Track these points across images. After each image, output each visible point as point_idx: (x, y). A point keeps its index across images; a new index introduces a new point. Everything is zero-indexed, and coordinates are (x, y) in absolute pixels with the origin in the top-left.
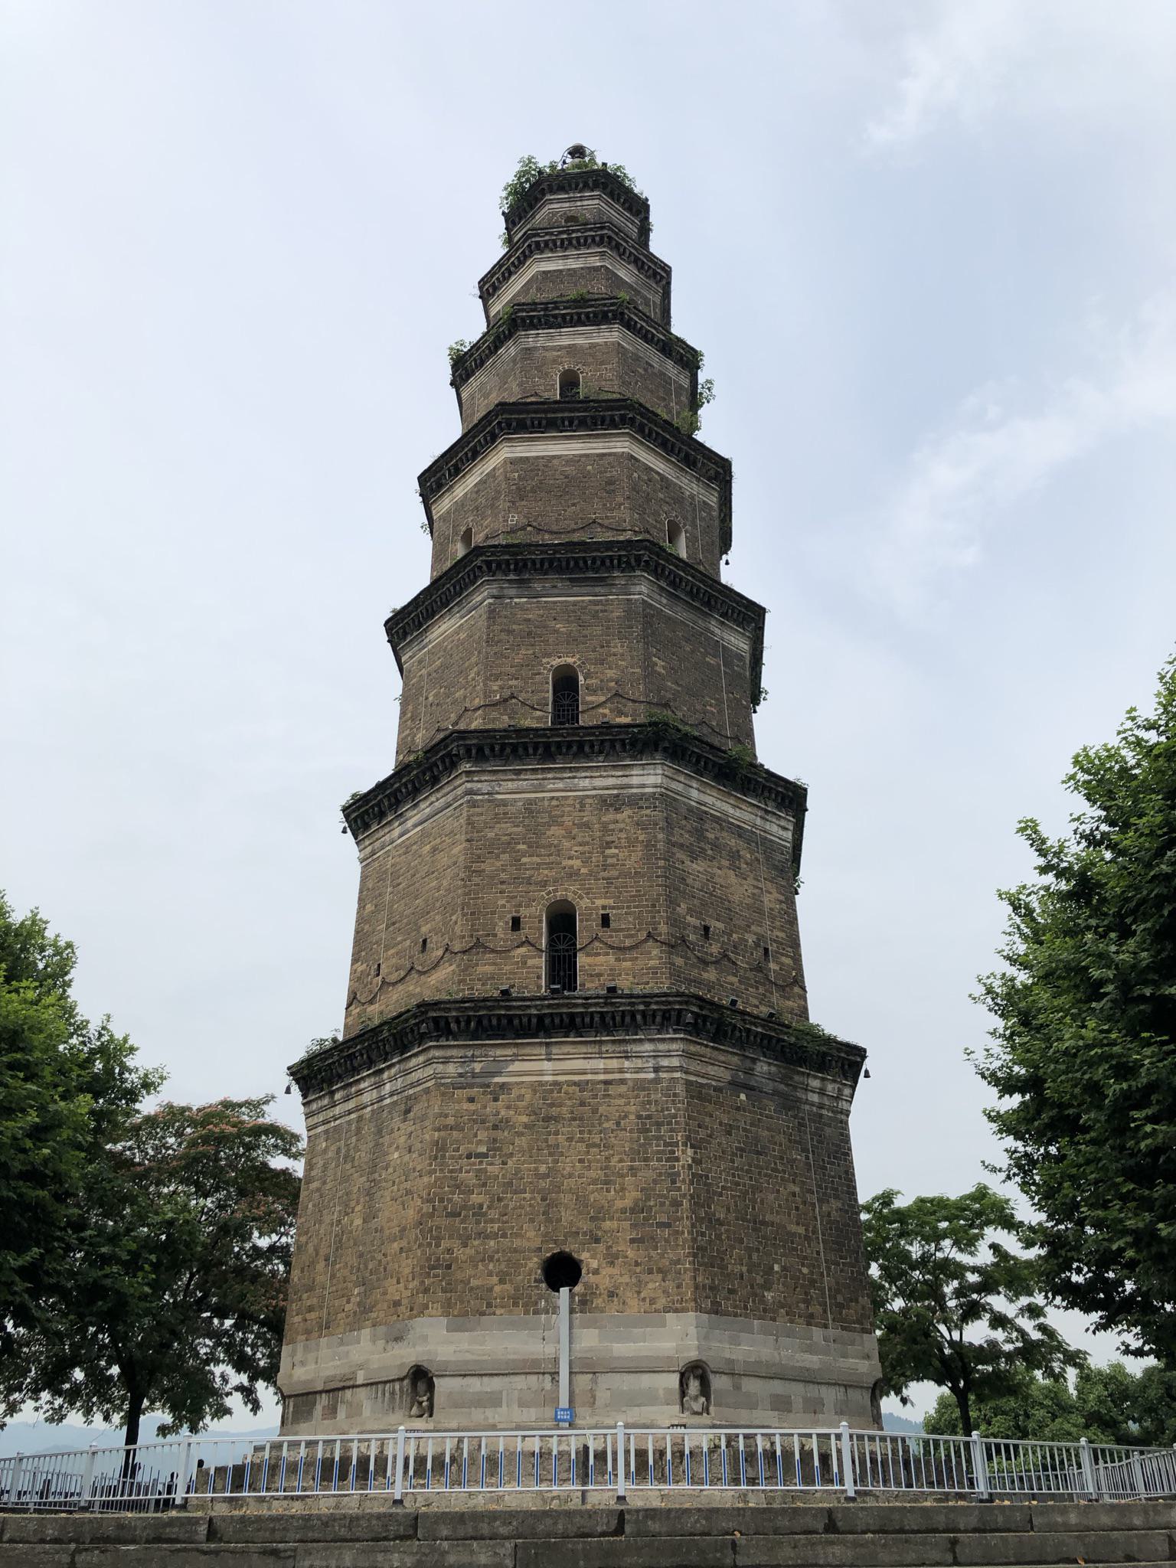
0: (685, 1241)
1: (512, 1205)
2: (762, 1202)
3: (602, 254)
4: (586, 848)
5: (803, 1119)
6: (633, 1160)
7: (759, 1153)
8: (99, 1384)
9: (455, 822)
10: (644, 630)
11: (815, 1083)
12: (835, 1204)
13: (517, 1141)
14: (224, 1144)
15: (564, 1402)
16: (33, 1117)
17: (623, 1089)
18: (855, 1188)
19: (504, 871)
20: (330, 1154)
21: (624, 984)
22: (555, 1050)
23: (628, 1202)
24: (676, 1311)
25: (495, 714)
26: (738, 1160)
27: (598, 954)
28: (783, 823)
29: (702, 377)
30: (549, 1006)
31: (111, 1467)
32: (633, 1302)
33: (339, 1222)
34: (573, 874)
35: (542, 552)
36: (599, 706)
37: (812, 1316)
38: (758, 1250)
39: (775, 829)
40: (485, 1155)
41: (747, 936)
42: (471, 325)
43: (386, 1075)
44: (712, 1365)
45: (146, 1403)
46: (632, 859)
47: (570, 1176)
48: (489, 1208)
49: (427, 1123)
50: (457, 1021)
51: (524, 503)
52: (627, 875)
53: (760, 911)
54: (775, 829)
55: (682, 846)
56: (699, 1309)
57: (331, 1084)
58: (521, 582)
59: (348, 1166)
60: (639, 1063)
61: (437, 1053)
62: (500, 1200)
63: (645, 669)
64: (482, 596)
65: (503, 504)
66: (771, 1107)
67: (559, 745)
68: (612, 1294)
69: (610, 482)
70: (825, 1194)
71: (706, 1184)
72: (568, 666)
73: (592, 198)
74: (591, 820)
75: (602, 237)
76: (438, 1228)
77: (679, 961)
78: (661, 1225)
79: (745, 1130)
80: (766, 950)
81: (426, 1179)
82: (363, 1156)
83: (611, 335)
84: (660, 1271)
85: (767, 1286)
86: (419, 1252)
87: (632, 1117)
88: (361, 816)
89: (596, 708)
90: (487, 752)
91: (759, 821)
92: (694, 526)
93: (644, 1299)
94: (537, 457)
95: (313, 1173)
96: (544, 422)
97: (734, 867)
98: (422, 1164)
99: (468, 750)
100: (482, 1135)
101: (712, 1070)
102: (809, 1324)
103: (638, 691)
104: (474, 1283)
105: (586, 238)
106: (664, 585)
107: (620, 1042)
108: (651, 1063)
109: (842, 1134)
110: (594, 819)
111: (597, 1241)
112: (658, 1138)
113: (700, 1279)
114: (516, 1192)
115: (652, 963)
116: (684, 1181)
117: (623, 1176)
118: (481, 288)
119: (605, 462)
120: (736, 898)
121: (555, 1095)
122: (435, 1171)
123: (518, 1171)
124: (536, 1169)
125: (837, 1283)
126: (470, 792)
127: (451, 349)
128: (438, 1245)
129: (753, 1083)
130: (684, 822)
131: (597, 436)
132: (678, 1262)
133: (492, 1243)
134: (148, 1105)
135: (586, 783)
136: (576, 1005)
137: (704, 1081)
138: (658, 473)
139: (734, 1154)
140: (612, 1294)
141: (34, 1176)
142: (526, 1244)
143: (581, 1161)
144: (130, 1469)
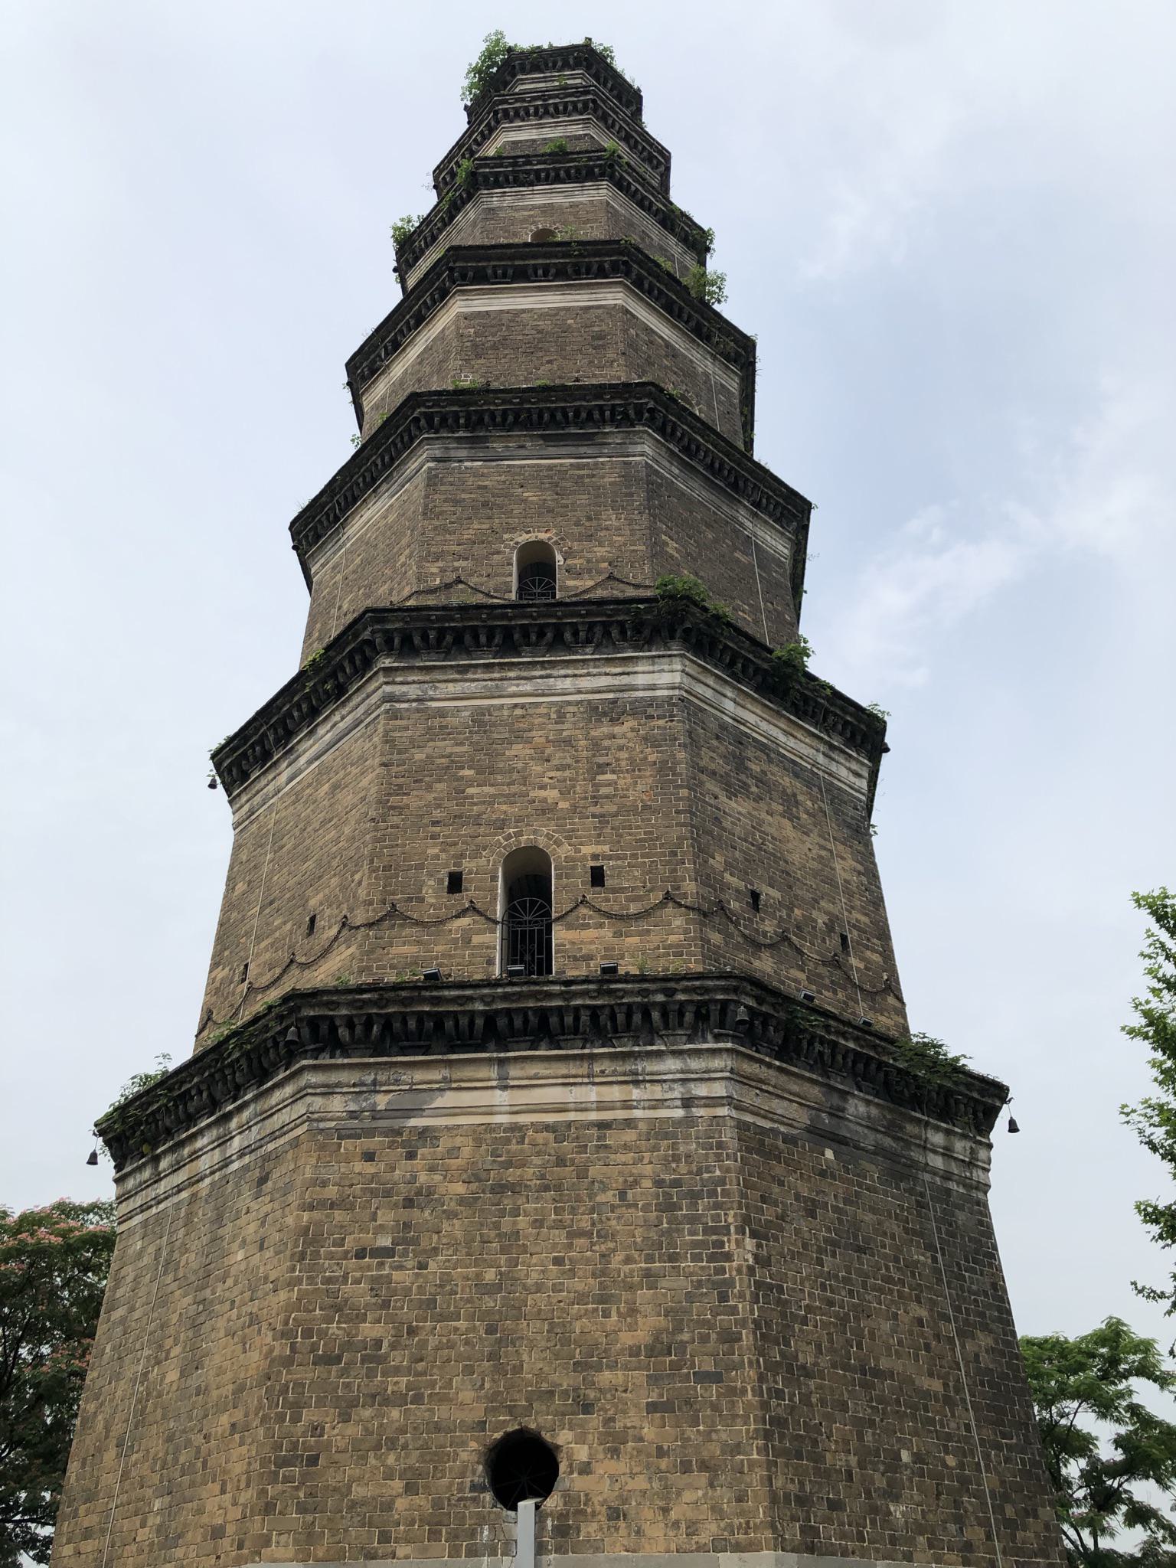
0: (748, 1406)
1: (433, 1341)
2: (872, 1333)
3: (586, 121)
4: (567, 773)
5: (922, 1195)
6: (650, 1259)
9: (366, 745)
10: (649, 499)
11: (937, 1139)
12: (985, 1340)
13: (446, 1226)
17: (630, 1136)
18: (1009, 1312)
19: (439, 806)
20: (146, 1260)
21: (628, 966)
22: (514, 1071)
23: (641, 1336)
24: (738, 1548)
26: (827, 1260)
27: (586, 926)
28: (854, 766)
30: (506, 997)
32: (655, 1530)
33: (145, 1375)
34: (546, 810)
35: (504, 402)
37: (968, 1547)
38: (872, 1423)
39: (843, 773)
40: (388, 1252)
41: (815, 914)
43: (234, 1124)
46: (639, 789)
47: (539, 1288)
48: (393, 1347)
49: (290, 1198)
50: (350, 1023)
51: (482, 361)
53: (831, 881)
54: (843, 773)
55: (714, 773)
56: (781, 1544)
58: (473, 442)
59: (169, 1279)
60: (657, 1092)
62: (412, 1332)
64: (420, 462)
66: (874, 1172)
68: (615, 1514)
69: (601, 336)
70: (966, 1322)
71: (779, 1302)
74: (573, 749)
76: (300, 1385)
77: (716, 938)
78: (703, 1377)
79: (836, 1209)
80: (844, 938)
81: (283, 1295)
82: (191, 1260)
84: (704, 1466)
86: (261, 1431)
87: (647, 1183)
88: (236, 763)
90: (417, 640)
91: (821, 759)
93: (676, 1524)
94: (502, 311)
96: (510, 272)
97: (793, 818)
99: (389, 642)
100: (386, 1217)
101: (779, 1107)
104: (358, 1492)
105: (566, 105)
106: (676, 450)
107: (625, 1056)
108: (678, 1091)
109: (981, 1223)
111: (587, 1408)
112: (693, 1220)
113: (778, 1483)
114: (443, 1318)
115: (673, 939)
116: (742, 1295)
117: (631, 1288)
118: (436, 178)
119: (593, 313)
120: (795, 858)
121: (514, 1147)
122: (299, 1280)
124: (478, 1276)
125: (1003, 1482)
126: (390, 698)
127: (396, 229)
128: (296, 1419)
129: (845, 1133)
130: (715, 743)
131: (581, 286)
132: (737, 1448)
133: (395, 1413)
135: (568, 683)
136: (550, 995)
137: (768, 1125)
138: (661, 337)
139: (820, 1250)
140: (615, 1514)
142: (458, 1416)
143: (558, 1261)
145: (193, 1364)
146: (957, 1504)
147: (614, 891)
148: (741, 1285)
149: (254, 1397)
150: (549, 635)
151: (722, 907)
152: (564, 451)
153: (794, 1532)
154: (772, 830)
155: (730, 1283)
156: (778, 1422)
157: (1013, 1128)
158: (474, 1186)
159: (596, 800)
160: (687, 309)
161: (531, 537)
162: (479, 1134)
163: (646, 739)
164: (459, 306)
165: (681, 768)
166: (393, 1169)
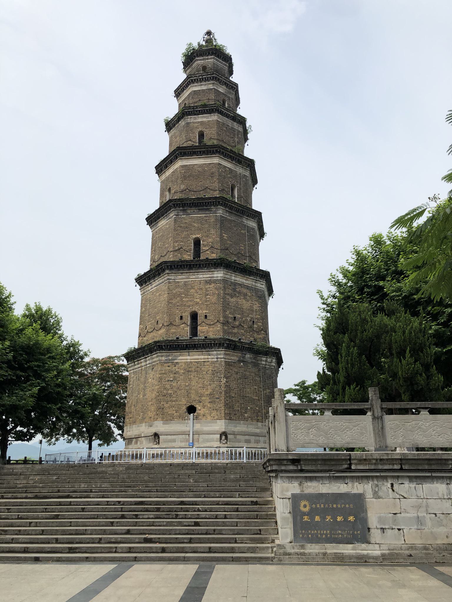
8: (80, 433)
9: (164, 287)
10: (221, 225)
11: (264, 359)
12: (268, 391)
14: (109, 371)
15: (191, 441)
16: (55, 373)
20: (135, 378)
22: (190, 353)
23: (208, 393)
25: (176, 254)
28: (262, 283)
29: (247, 125)
31: (85, 455)
32: (209, 417)
34: (197, 303)
36: (207, 250)
37: (258, 420)
39: (259, 285)
40: (172, 381)
42: (172, 108)
44: (228, 432)
45: (94, 438)
46: (214, 299)
49: (157, 372)
50: (165, 346)
53: (253, 311)
54: (259, 285)
57: (134, 360)
60: (213, 357)
61: (160, 354)
63: (221, 238)
64: (172, 215)
65: (179, 181)
67: (194, 265)
68: (204, 415)
72: (198, 237)
73: (211, 58)
74: (203, 287)
75: (213, 77)
77: (226, 328)
78: (217, 398)
80: (253, 322)
82: (142, 379)
83: (214, 117)
85: (246, 413)
92: (240, 184)
97: (245, 298)
98: (156, 383)
99: (168, 266)
101: (232, 358)
103: (218, 246)
104: (169, 413)
110: (204, 287)
111: (200, 402)
115: (218, 329)
123: (181, 384)
126: (169, 279)
132: (221, 407)
134: (87, 360)
135: (201, 276)
138: (228, 168)
140: (204, 415)
141: (58, 385)
142: (182, 403)
144: (89, 456)
149: (154, 400)
152: (204, 212)
160: (235, 157)
162: (185, 363)
164: (179, 163)
165: (222, 295)
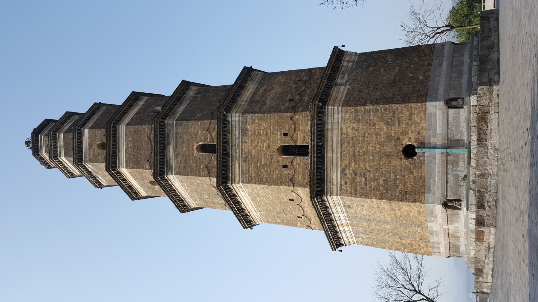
1: (384, 169)
2: (387, 80)
6: (370, 125)
7: (369, 82)
10: (186, 120)
11: (345, 64)
12: (388, 56)
17: (344, 129)
23: (385, 127)
24: (426, 109)
34: (269, 146)
35: (157, 155)
36: (211, 136)
37: (429, 64)
38: (404, 82)
40: (366, 178)
41: (293, 87)
46: (265, 125)
48: (385, 177)
52: (270, 126)
63: (199, 120)
67: (223, 150)
68: (419, 133)
77: (301, 109)
78: (394, 115)
79: (361, 86)
80: (299, 81)
84: (411, 115)
87: (354, 125)
89: (212, 138)
94: (126, 157)
95: (370, 242)
97: (270, 91)
102: (431, 65)
103: (207, 122)
104: (412, 183)
113: (414, 101)
114: (380, 167)
118: (70, 178)
132: (408, 109)
133: (398, 176)
140: (419, 133)
143: (369, 144)
145: (386, 222)
146: (420, 66)
147: (289, 131)
148: (376, 107)
150: (225, 145)
151: (293, 108)
153: (423, 98)
154: (274, 95)
155: (376, 109)
156: (403, 101)
157: (343, 46)
158: (353, 161)
159: (267, 134)
161: (195, 149)
163: (252, 123)
164: (125, 171)
166: (349, 178)
